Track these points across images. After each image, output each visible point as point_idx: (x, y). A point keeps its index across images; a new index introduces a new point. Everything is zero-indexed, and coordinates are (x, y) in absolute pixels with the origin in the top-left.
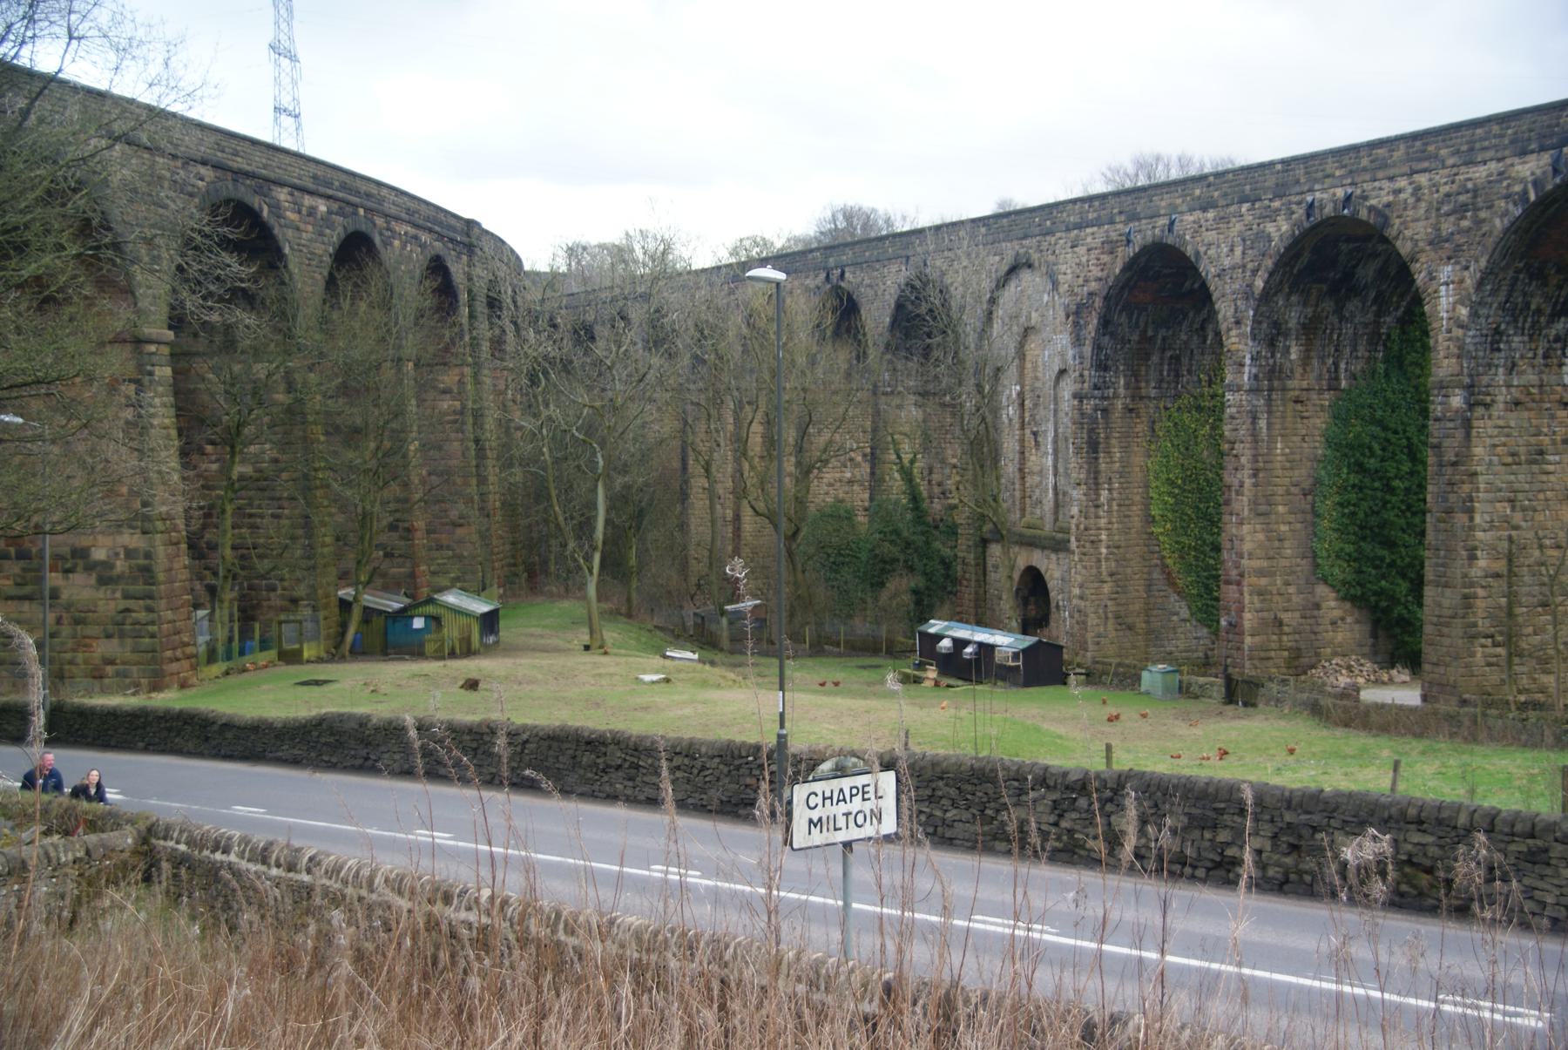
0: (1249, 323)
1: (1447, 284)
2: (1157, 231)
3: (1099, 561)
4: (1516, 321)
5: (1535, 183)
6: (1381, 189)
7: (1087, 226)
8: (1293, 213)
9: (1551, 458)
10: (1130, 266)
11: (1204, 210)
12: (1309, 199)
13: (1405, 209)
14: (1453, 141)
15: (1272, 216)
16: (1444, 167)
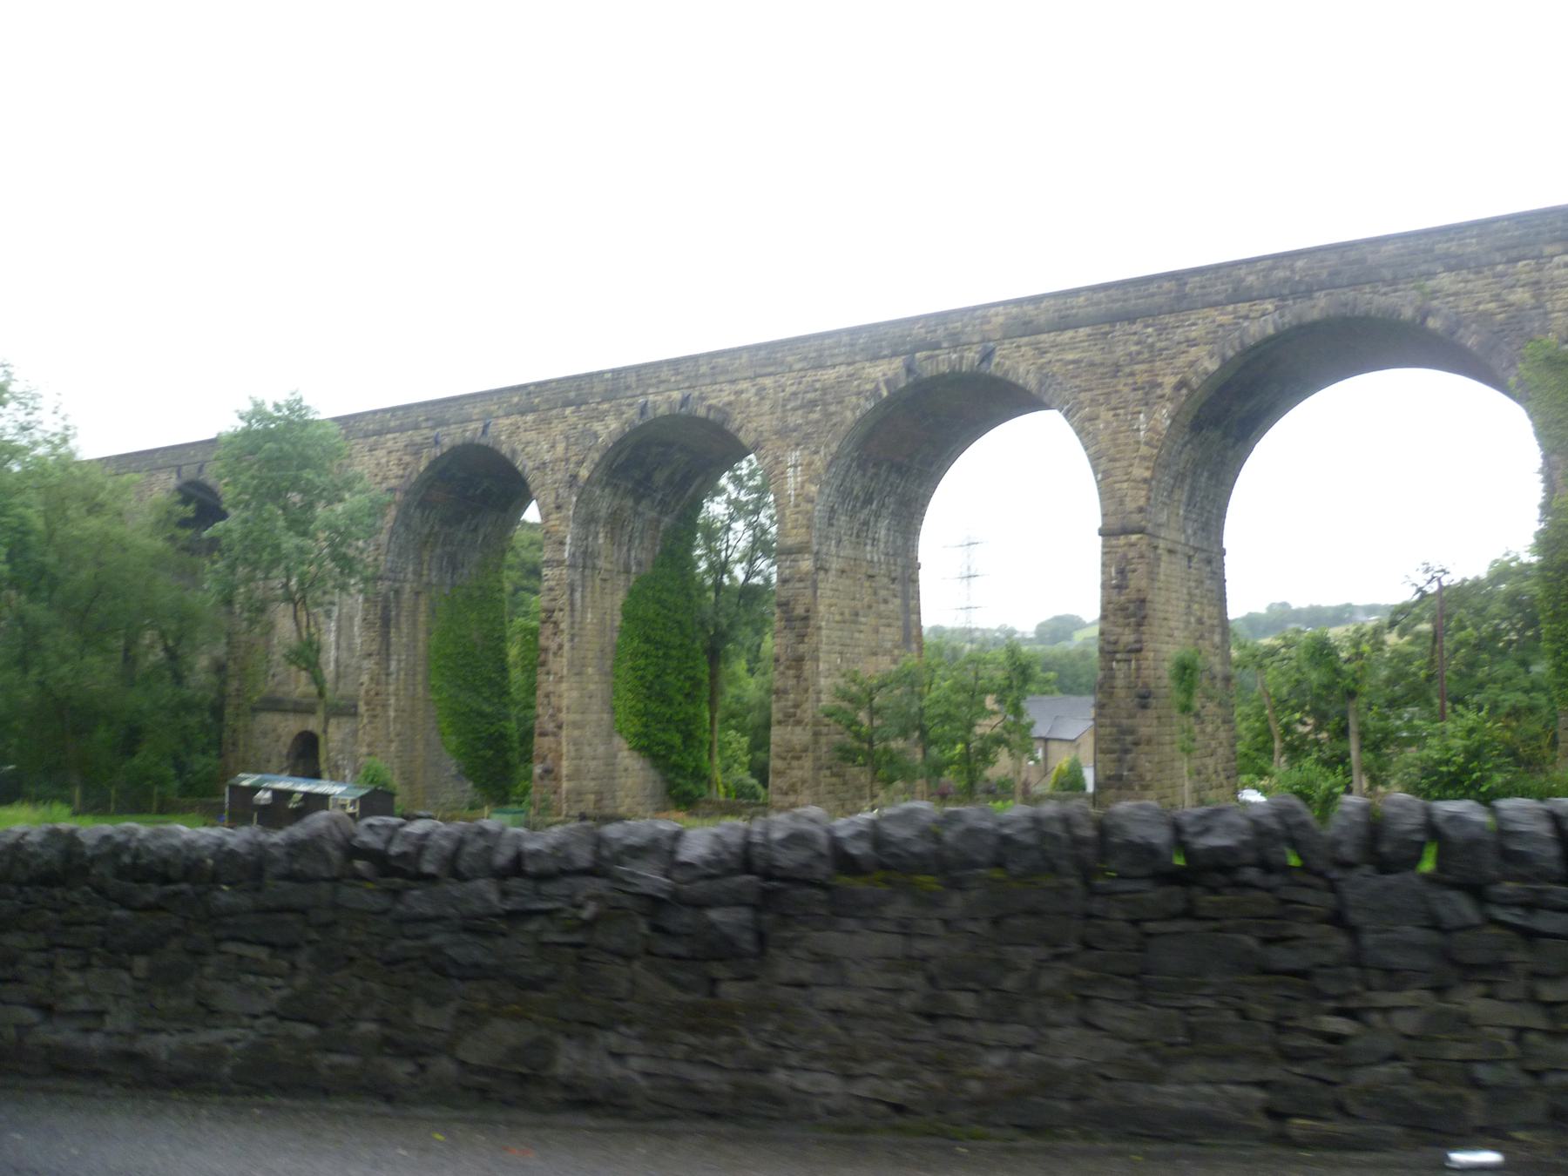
0: (572, 508)
1: (795, 466)
2: (468, 434)
3: (387, 722)
4: (844, 503)
5: (887, 382)
6: (721, 391)
7: (387, 433)
8: (623, 413)
9: (863, 620)
10: (433, 464)
11: (523, 413)
12: (641, 400)
13: (748, 406)
14: (799, 351)
15: (601, 417)
16: (791, 371)
